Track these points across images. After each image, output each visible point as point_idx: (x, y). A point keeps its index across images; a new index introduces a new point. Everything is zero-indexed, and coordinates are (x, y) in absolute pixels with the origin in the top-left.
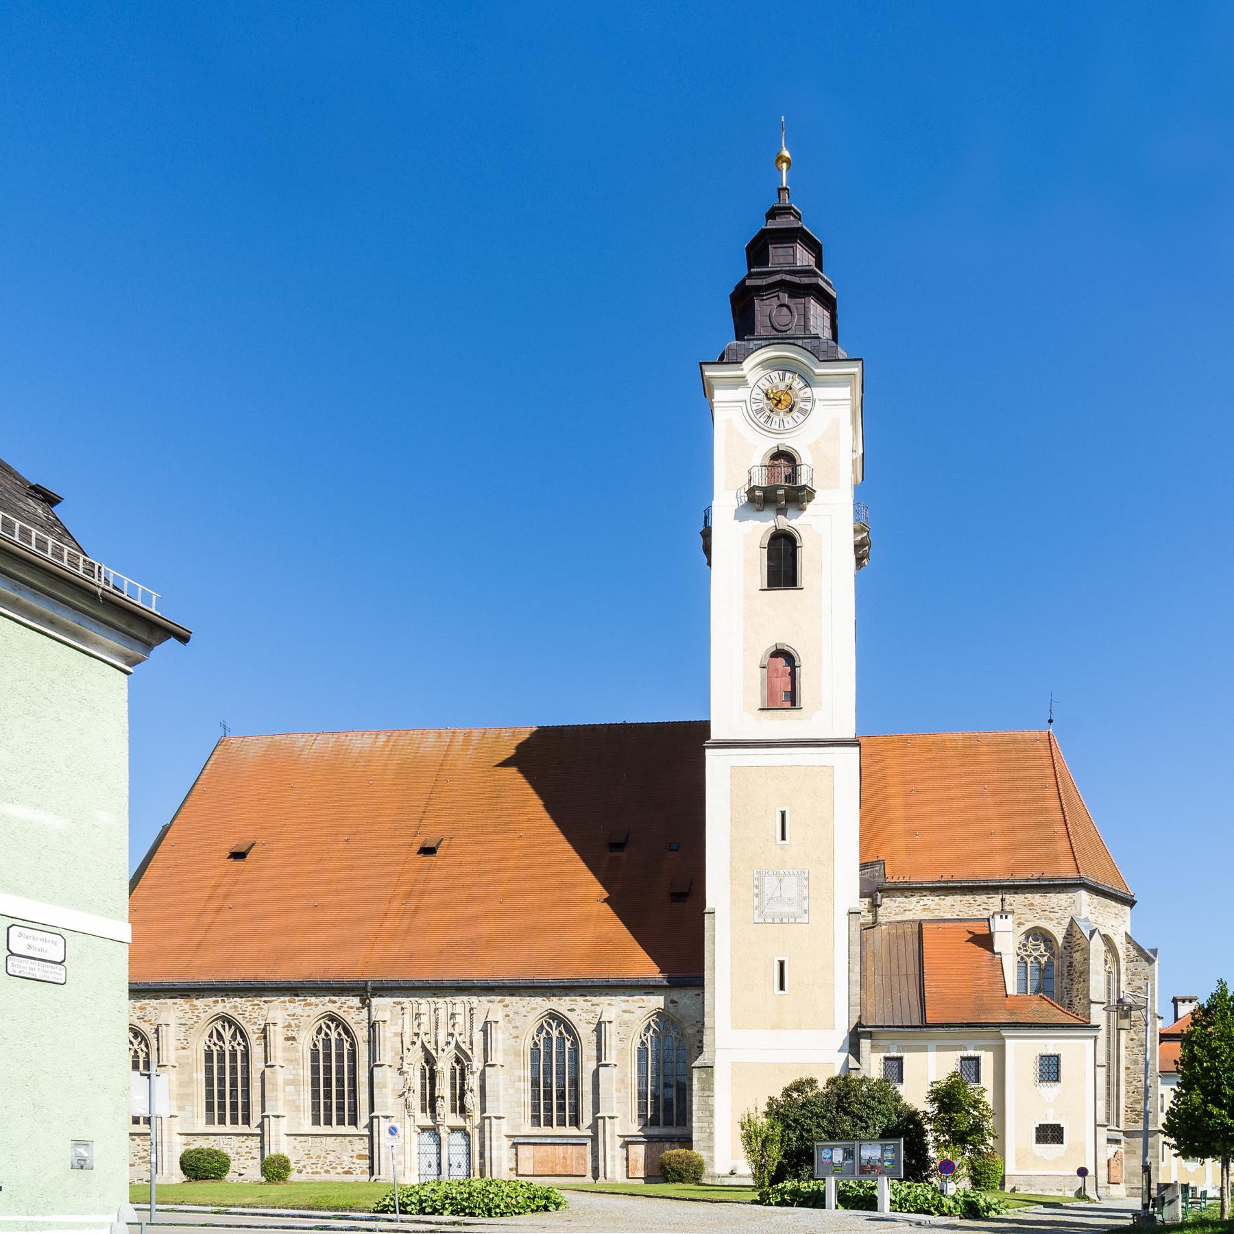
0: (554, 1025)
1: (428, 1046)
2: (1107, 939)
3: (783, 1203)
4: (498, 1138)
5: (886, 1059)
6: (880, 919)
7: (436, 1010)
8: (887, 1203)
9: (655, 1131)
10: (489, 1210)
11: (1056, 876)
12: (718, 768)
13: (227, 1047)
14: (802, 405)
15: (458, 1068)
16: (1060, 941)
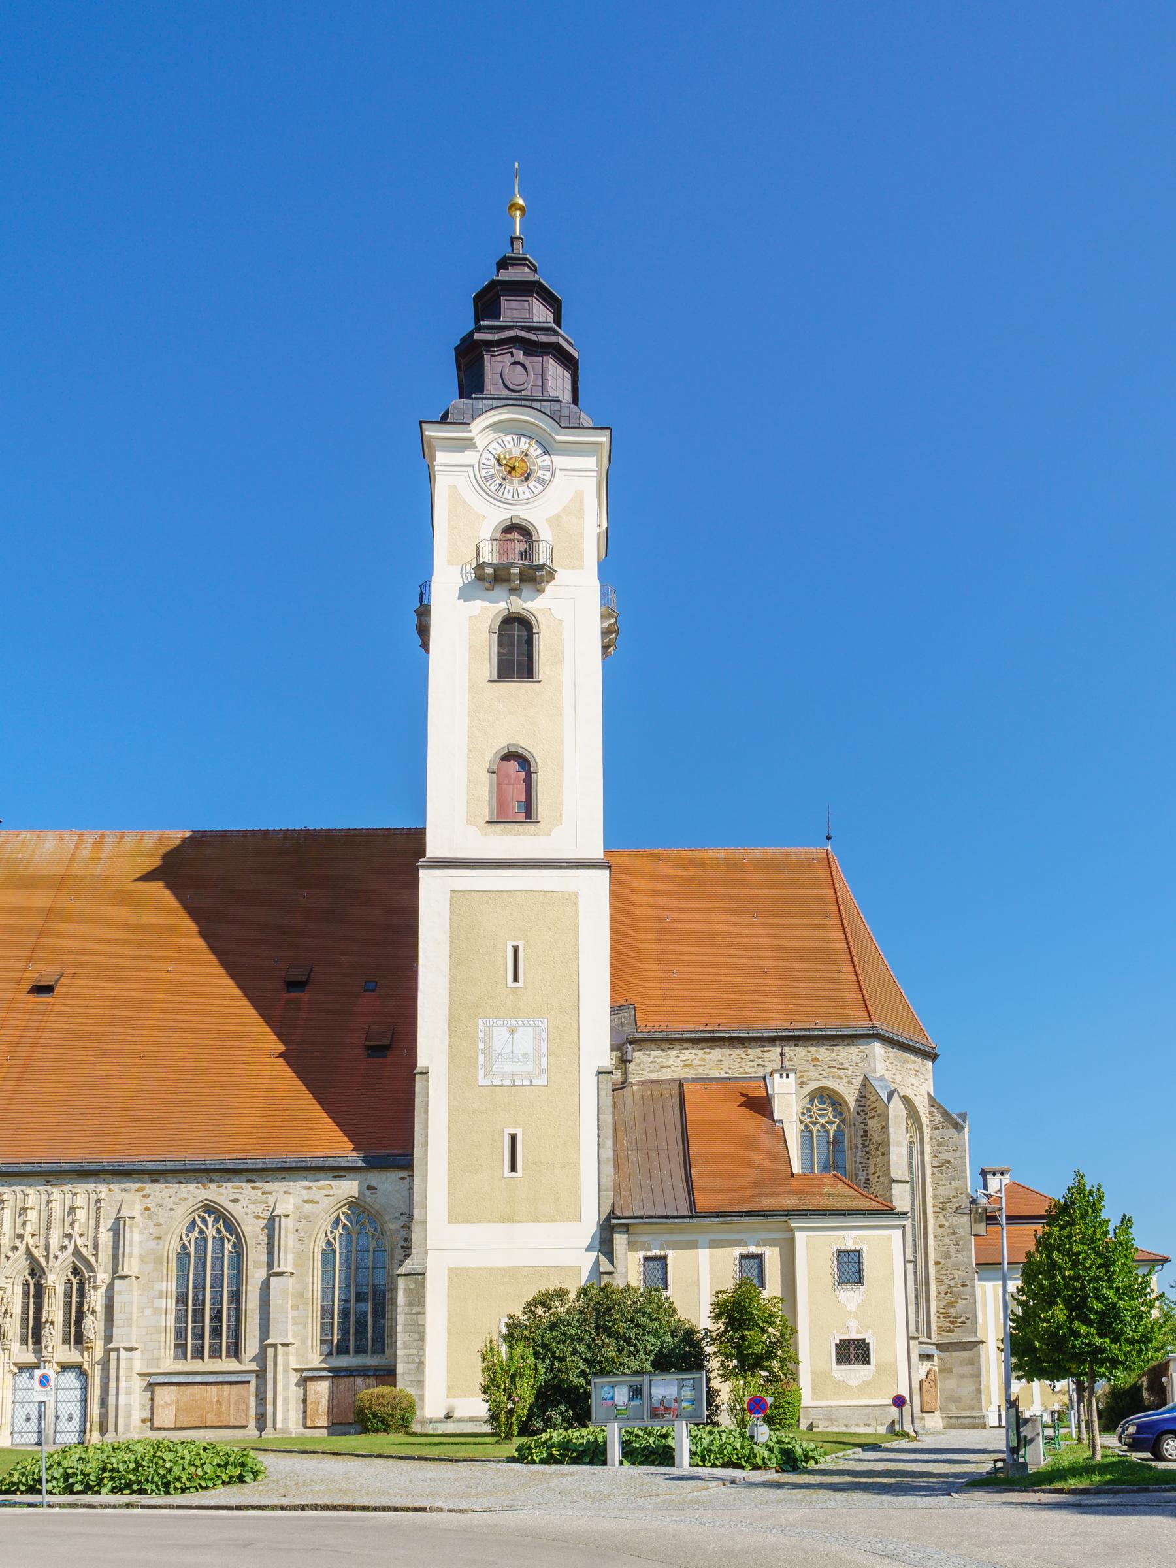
0: (210, 1221)
1: (35, 1251)
2: (906, 1100)
3: (549, 1460)
4: (128, 1378)
5: (647, 1259)
6: (632, 1078)
7: (49, 1202)
8: (687, 1455)
9: (343, 1362)
10: (167, 1485)
11: (844, 1024)
12: (434, 892)
14: (540, 473)
15: (75, 1281)
16: (852, 1104)
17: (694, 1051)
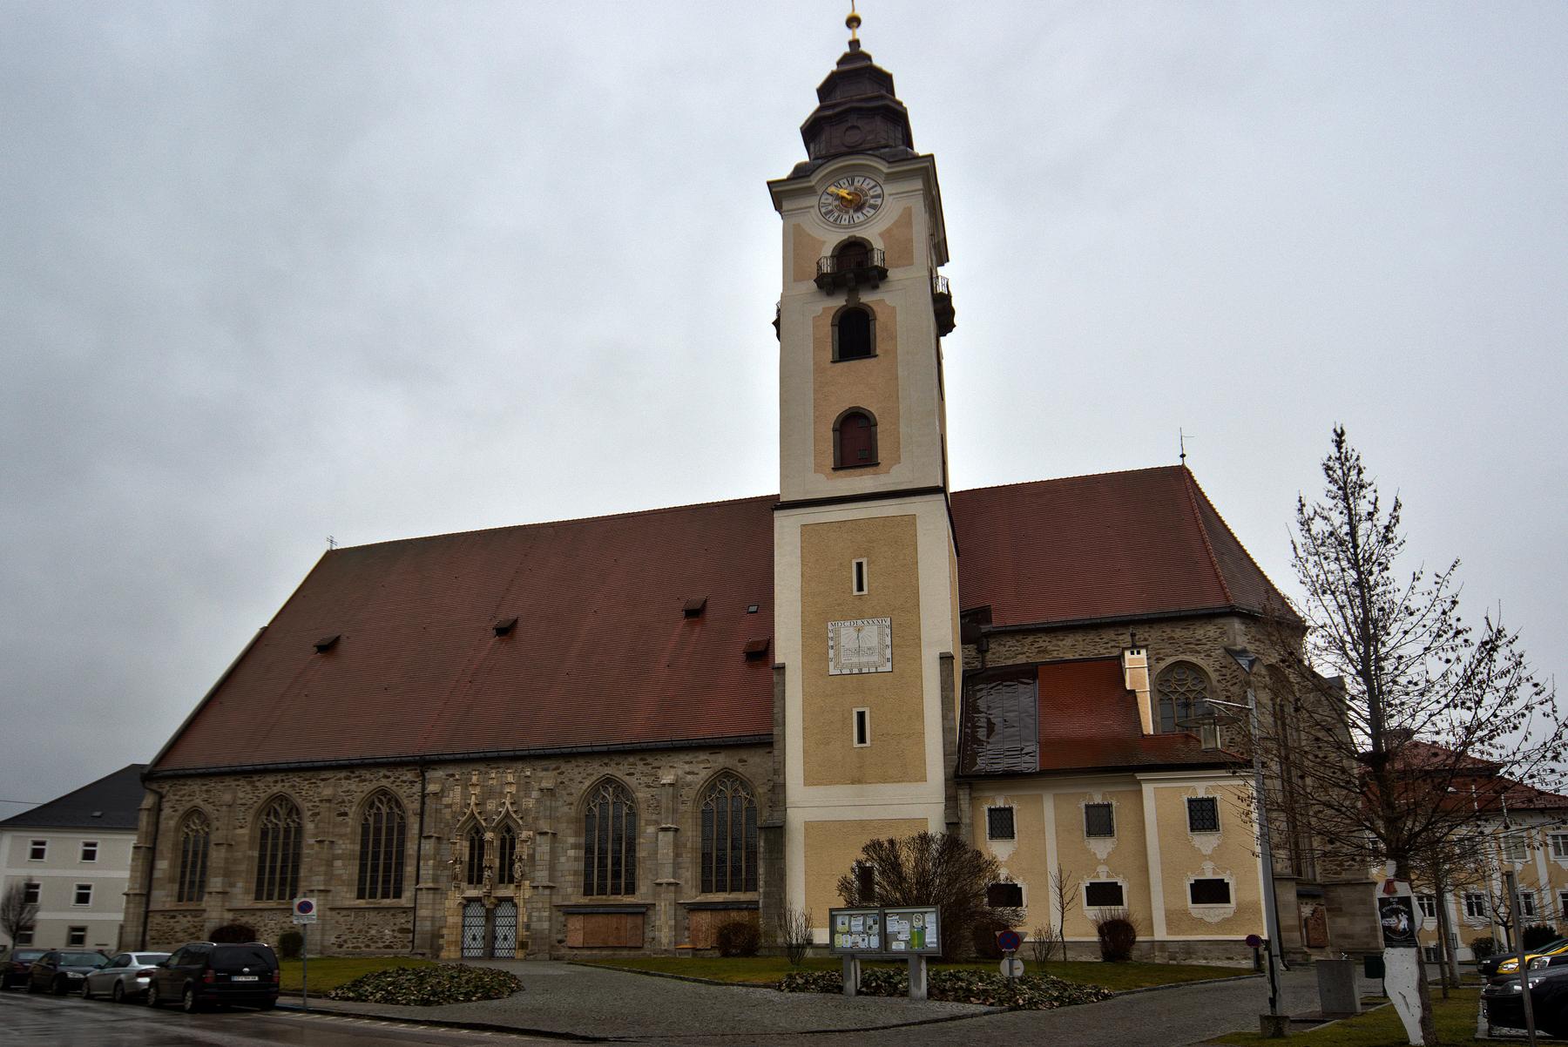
13: (282, 825)
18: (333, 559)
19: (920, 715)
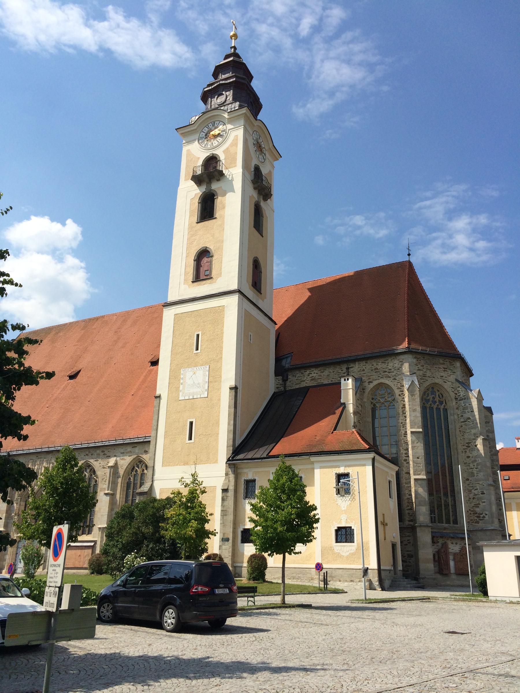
17: (316, 372)
18: (212, 75)
19: (217, 423)
